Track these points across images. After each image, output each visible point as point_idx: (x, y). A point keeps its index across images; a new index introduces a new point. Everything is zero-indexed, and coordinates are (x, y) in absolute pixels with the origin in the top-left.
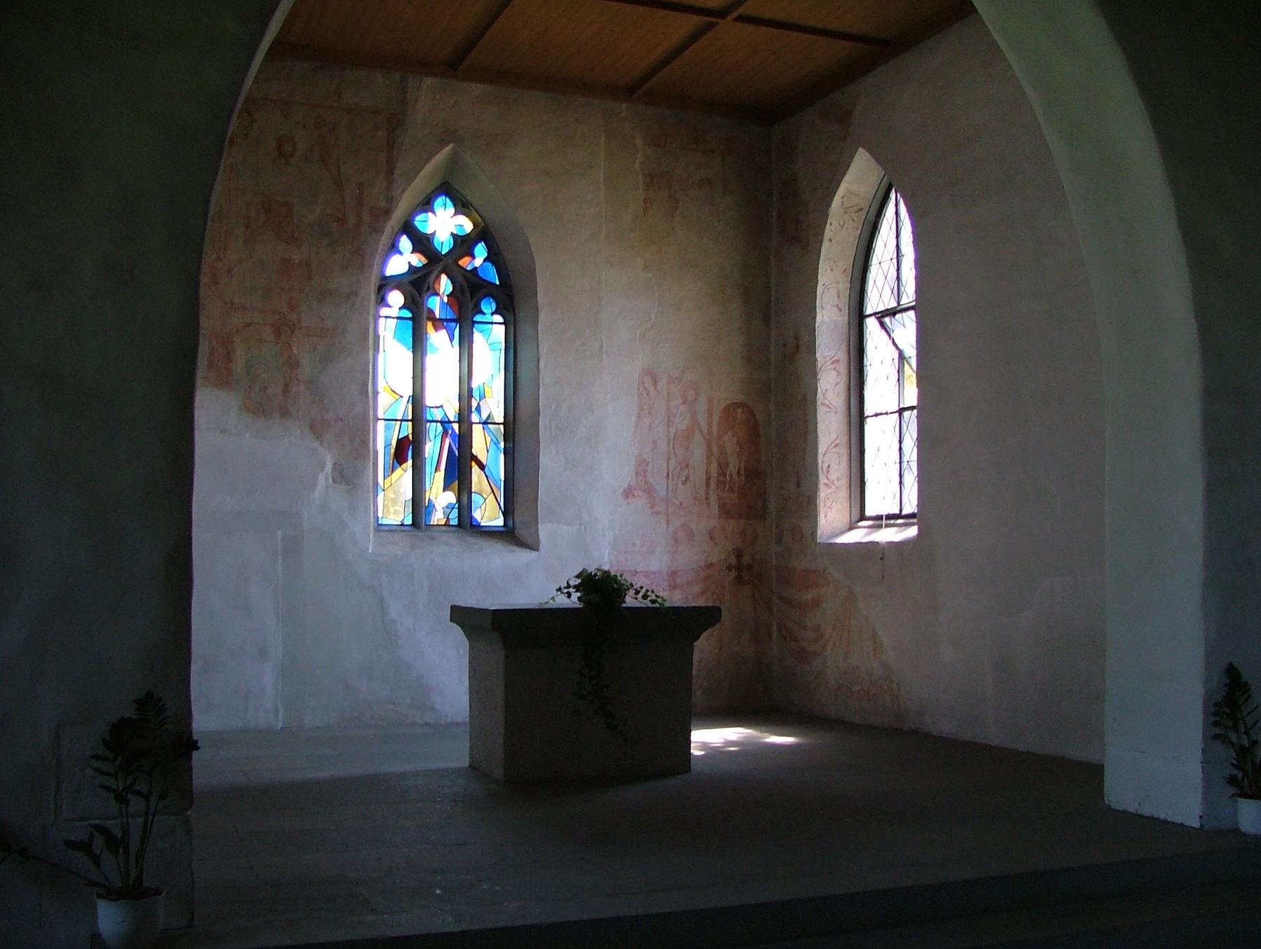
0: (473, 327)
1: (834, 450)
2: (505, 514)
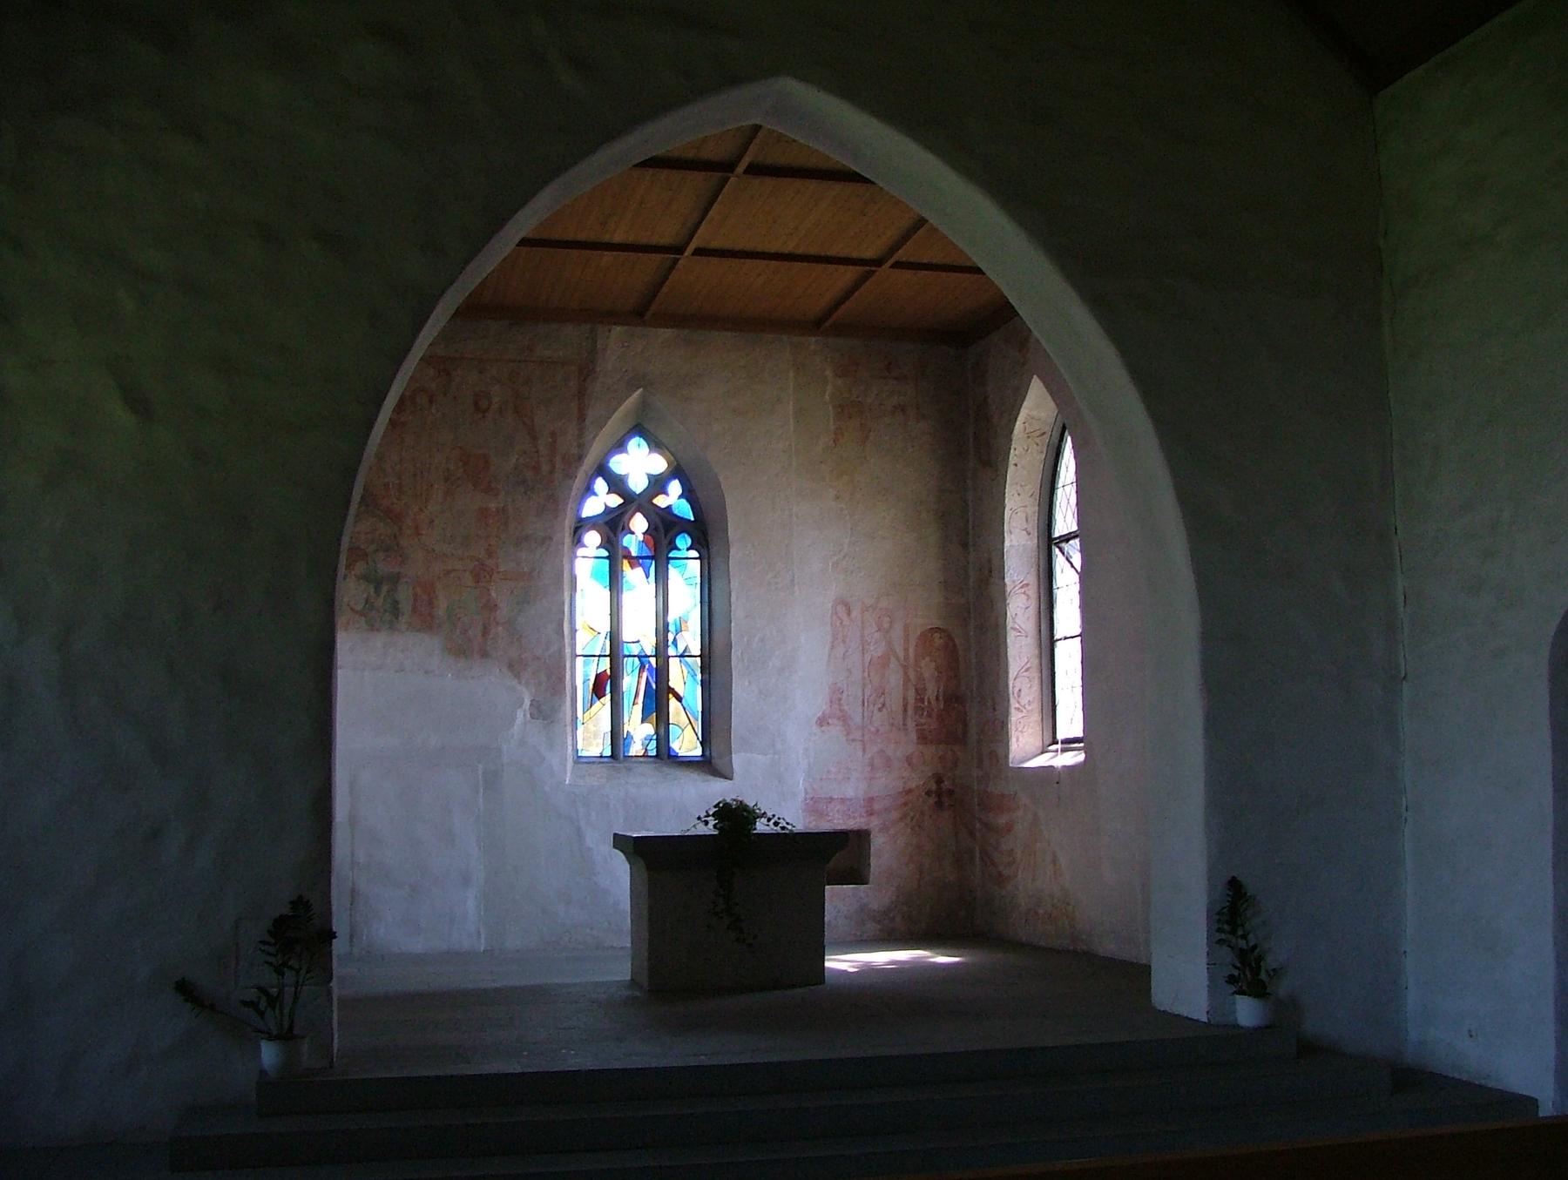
0: (668, 563)
1: (1025, 674)
2: (704, 742)
